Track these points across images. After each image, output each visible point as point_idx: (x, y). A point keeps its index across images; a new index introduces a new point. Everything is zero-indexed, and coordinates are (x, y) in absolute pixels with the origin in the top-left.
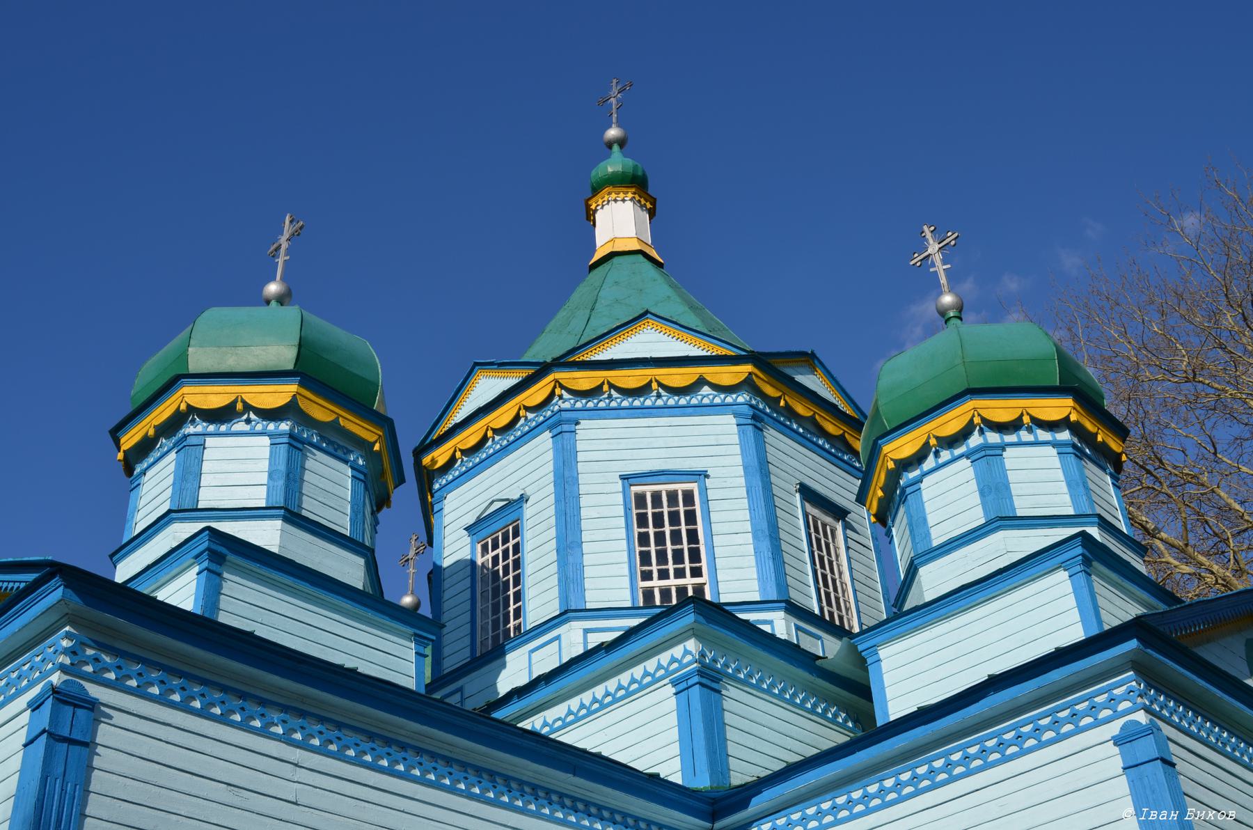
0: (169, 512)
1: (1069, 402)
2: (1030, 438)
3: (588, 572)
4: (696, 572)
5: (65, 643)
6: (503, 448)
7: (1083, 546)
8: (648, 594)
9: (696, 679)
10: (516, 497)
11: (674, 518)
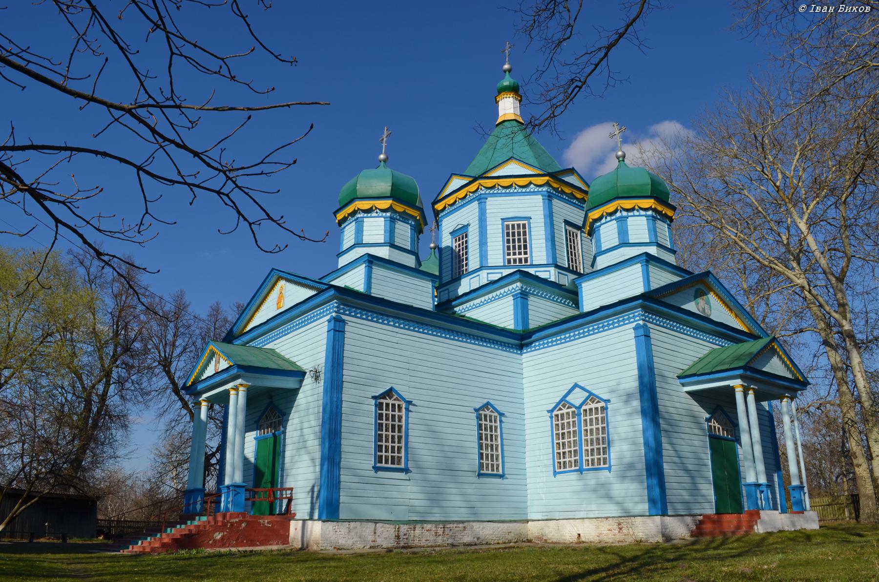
1: (652, 201)
2: (638, 214)
3: (489, 253)
4: (526, 253)
5: (335, 305)
6: (462, 205)
7: (646, 256)
8: (509, 261)
9: (519, 295)
10: (466, 224)
11: (519, 234)
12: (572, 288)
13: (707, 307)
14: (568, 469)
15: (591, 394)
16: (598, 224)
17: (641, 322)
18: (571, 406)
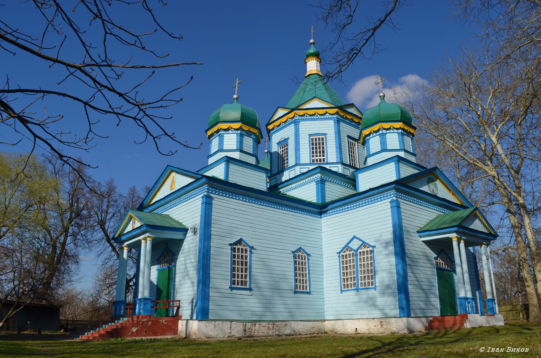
0: (218, 150)
1: (401, 123)
2: (392, 131)
3: (301, 155)
4: (323, 156)
5: (206, 187)
6: (284, 126)
7: (398, 158)
8: (313, 160)
9: (320, 182)
10: (287, 138)
11: (319, 144)
12: (352, 177)
13: (435, 189)
14: (349, 288)
15: (364, 242)
16: (368, 138)
17: (395, 198)
18: (351, 250)
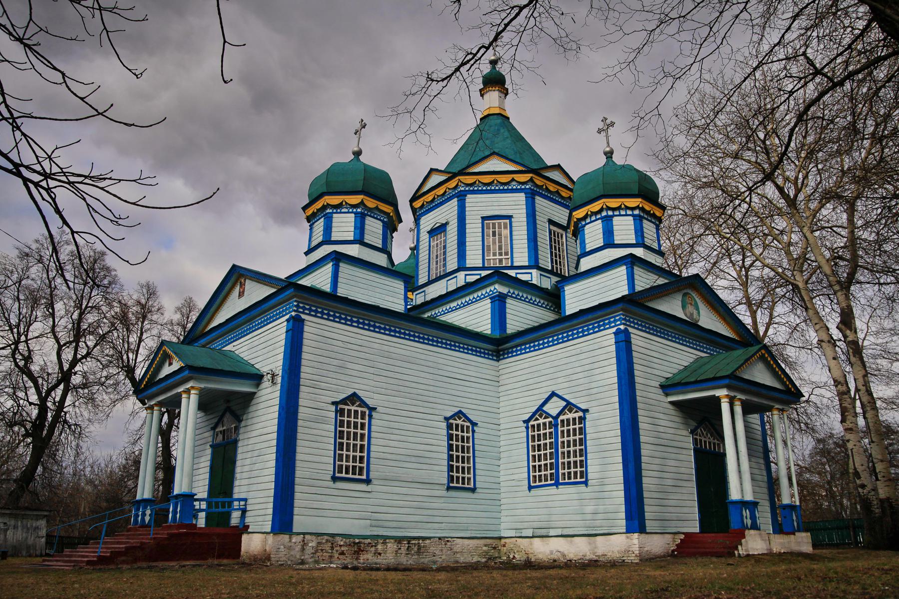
1: (640, 200)
6: (441, 203)
9: (497, 298)
13: (695, 312)
14: (543, 483)
15: (569, 403)
16: (583, 223)
17: (622, 327)
18: (548, 415)
